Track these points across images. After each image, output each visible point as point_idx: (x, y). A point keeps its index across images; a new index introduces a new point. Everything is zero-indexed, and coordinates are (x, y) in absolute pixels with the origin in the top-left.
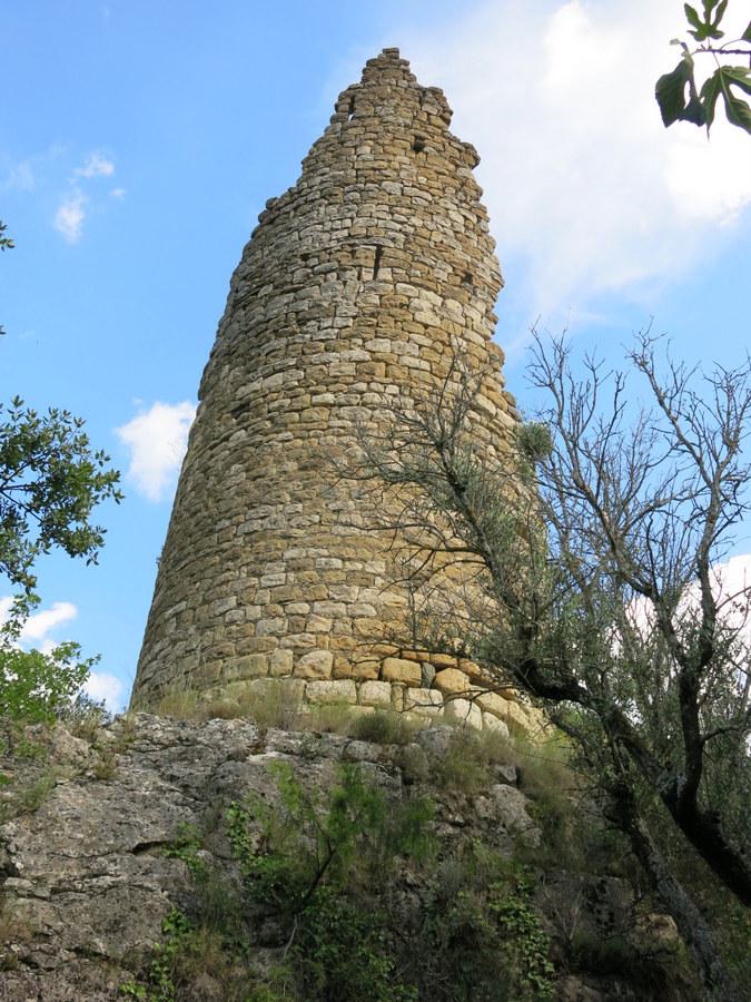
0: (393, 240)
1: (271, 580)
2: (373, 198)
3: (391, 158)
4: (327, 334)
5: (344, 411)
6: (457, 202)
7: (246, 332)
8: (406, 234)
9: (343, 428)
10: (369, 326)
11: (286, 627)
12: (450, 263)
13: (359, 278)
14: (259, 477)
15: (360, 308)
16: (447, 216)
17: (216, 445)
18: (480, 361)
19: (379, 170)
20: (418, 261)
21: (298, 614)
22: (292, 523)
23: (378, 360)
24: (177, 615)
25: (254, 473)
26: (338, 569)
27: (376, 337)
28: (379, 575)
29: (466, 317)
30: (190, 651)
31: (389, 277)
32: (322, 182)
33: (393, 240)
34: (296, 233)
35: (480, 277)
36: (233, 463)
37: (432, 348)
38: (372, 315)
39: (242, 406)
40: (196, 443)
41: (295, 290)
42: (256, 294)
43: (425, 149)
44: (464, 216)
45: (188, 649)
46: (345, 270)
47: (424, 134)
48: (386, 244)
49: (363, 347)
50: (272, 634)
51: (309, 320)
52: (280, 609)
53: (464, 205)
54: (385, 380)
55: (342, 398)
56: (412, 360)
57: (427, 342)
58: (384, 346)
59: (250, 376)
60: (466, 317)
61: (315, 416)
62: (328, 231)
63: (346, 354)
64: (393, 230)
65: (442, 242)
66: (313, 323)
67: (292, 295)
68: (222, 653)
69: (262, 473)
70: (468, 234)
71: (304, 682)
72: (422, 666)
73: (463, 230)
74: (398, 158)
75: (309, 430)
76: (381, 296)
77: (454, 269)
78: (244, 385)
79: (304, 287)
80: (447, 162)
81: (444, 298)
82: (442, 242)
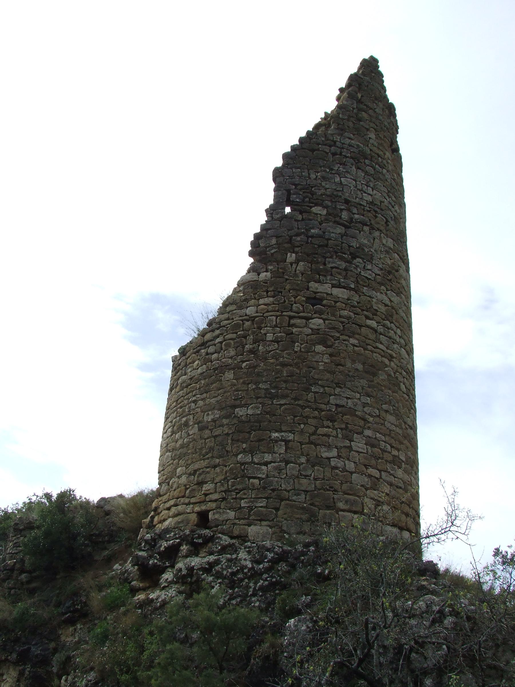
1: (358, 447)
36: (319, 344)
50: (362, 486)
68: (332, 487)
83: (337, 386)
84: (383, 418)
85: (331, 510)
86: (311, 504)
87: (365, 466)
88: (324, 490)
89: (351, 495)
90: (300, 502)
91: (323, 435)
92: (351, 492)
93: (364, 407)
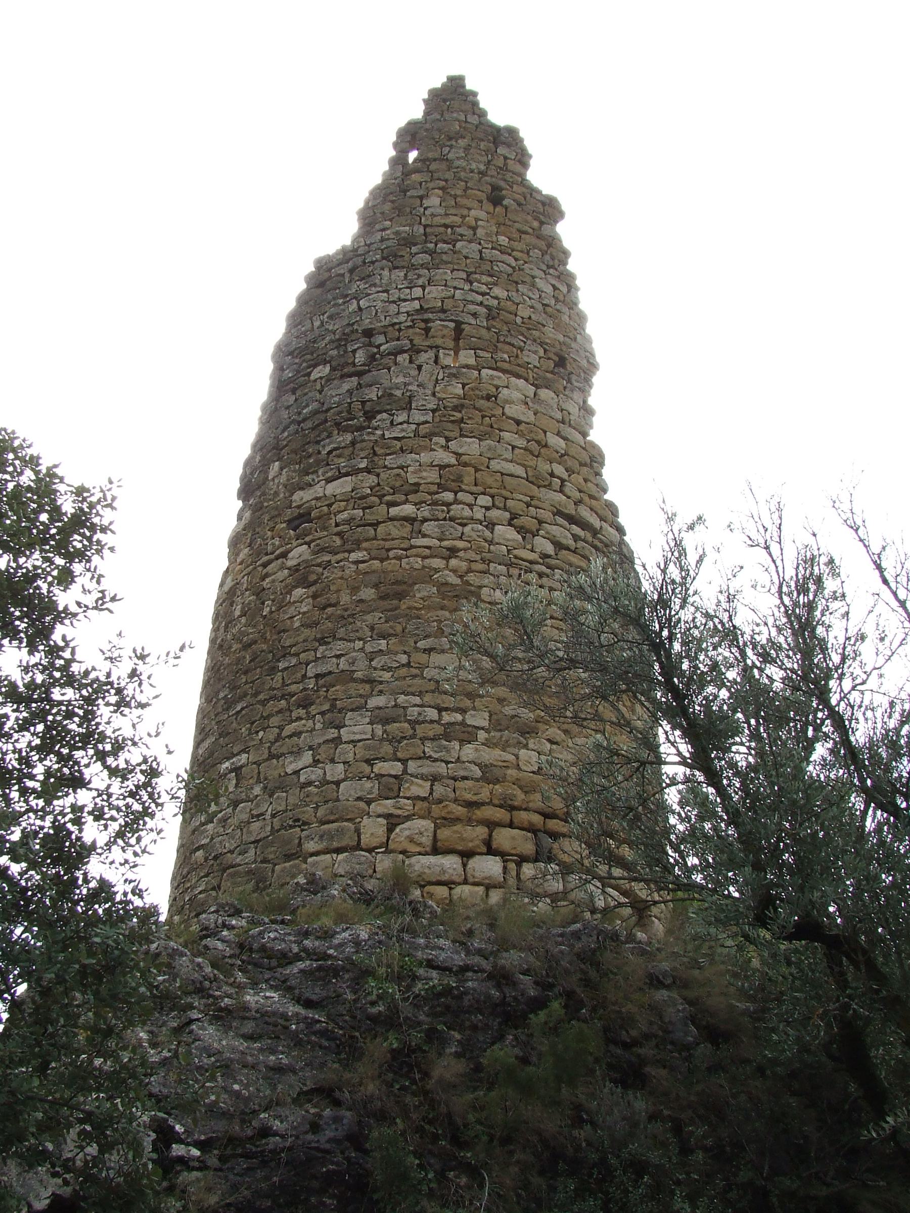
0: (475, 315)
1: (354, 733)
2: (447, 263)
3: (465, 212)
4: (403, 430)
5: (428, 527)
6: (544, 268)
7: (299, 423)
8: (487, 307)
9: (429, 548)
10: (453, 422)
11: (376, 791)
12: (541, 344)
13: (436, 362)
14: (330, 605)
15: (439, 399)
16: (533, 285)
17: (269, 562)
18: (581, 465)
19: (452, 227)
20: (505, 342)
21: (390, 776)
22: (374, 663)
23: (465, 465)
24: (237, 770)
25: (322, 600)
26: (432, 722)
27: (462, 436)
28: (483, 728)
29: (562, 410)
30: (258, 816)
31: (472, 361)
32: (382, 240)
33: (475, 315)
34: (355, 301)
35: (575, 360)
36: (296, 587)
37: (525, 449)
38: (456, 408)
39: (301, 516)
40: (242, 556)
41: (360, 374)
42: (309, 374)
43: (505, 202)
44: (553, 286)
45: (254, 812)
46: (418, 352)
47: (502, 184)
48: (466, 320)
49: (446, 448)
50: (359, 799)
51: (380, 412)
52: (367, 769)
53: (551, 271)
54: (474, 489)
55: (425, 512)
56: (504, 463)
57: (521, 443)
58: (471, 447)
59: (309, 478)
60: (562, 410)
61: (395, 533)
62: (394, 302)
63: (425, 457)
64: (473, 302)
65: (530, 318)
66: (385, 415)
67: (355, 379)
68: (298, 820)
69: (333, 601)
70: (558, 307)
71: (401, 856)
72: (536, 836)
73: (553, 302)
74: (473, 212)
75: (388, 550)
76: (464, 385)
77: (545, 351)
78: (302, 489)
79: (369, 371)
80: (529, 218)
81: (537, 387)
82: (530, 318)
83: (320, 645)
84: (417, 665)
85: (294, 859)
86: (262, 862)
87: (368, 762)
88: (285, 829)
89: (333, 822)
90: (246, 864)
91: (290, 737)
92: (332, 818)
93: (371, 660)
